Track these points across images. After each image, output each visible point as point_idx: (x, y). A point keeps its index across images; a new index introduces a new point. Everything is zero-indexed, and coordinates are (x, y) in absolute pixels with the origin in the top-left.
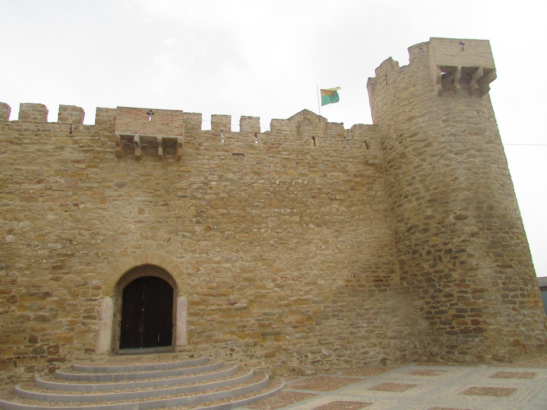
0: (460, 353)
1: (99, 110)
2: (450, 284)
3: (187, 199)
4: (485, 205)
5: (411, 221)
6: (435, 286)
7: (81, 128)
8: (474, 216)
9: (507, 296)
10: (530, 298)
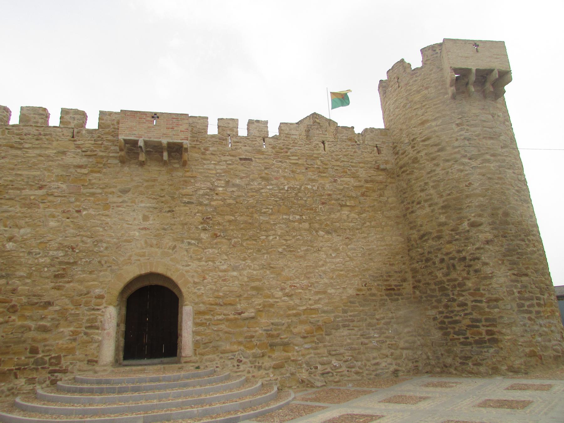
0: (474, 365)
1: (102, 113)
2: (464, 293)
3: (193, 206)
4: (500, 212)
5: (424, 228)
6: (449, 295)
7: (84, 132)
8: (489, 223)
9: (523, 305)
10: (546, 308)
